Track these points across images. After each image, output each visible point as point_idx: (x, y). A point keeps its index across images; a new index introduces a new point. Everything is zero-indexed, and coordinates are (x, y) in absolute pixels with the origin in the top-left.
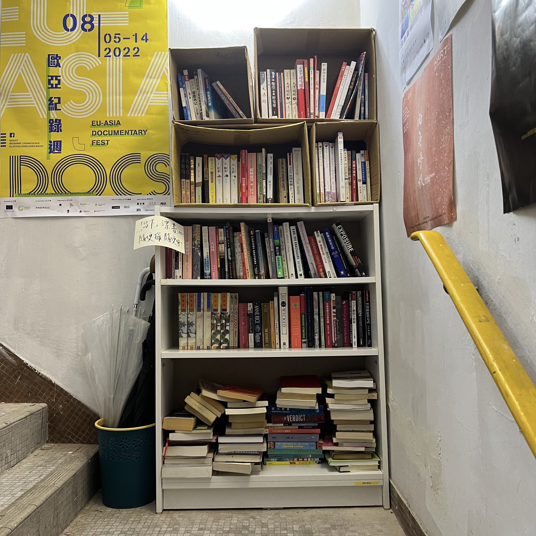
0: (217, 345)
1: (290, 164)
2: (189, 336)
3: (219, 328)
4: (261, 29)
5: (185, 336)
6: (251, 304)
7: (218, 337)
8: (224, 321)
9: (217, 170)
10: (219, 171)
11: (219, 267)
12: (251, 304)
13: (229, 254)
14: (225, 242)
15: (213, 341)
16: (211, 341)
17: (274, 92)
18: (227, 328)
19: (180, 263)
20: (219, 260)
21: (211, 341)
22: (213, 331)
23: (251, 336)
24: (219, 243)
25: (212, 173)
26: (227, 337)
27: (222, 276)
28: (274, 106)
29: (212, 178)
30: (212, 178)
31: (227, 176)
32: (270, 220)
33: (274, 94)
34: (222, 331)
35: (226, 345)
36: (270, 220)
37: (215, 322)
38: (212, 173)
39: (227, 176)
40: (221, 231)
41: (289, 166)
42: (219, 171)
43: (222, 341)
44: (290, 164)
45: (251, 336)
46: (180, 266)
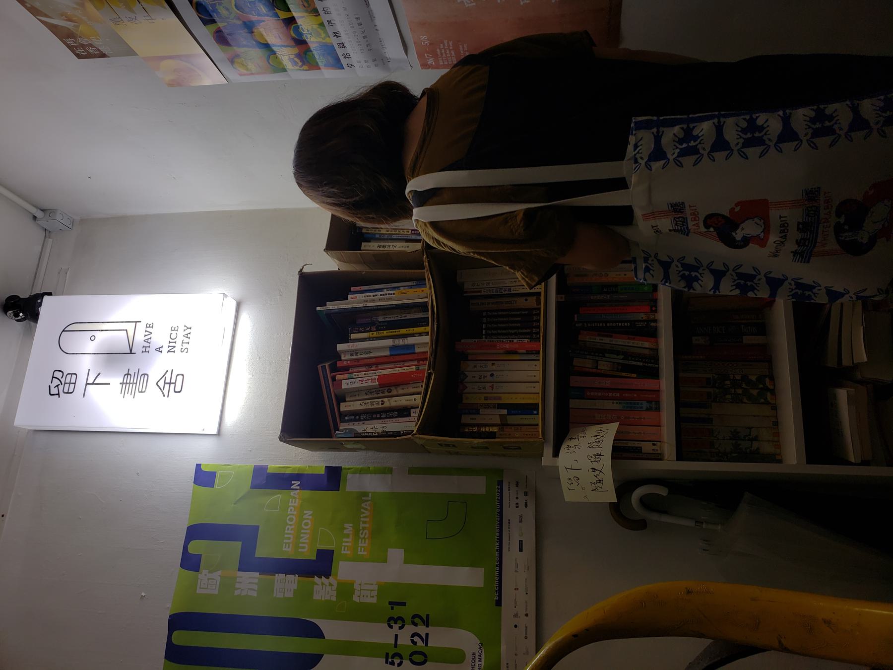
0: (769, 394)
1: (480, 292)
2: (756, 439)
3: (740, 391)
4: (283, 430)
5: (755, 445)
6: (694, 338)
7: (754, 392)
8: (728, 382)
9: (483, 391)
10: (484, 388)
11: (635, 375)
12: (694, 338)
13: (615, 356)
14: (597, 358)
15: (762, 400)
16: (762, 403)
17: (374, 416)
18: (738, 377)
19: (631, 444)
20: (624, 374)
21: (762, 403)
22: (745, 400)
23: (747, 340)
24: (597, 368)
25: (486, 398)
26: (754, 378)
27: (655, 374)
28: (396, 414)
29: (495, 398)
30: (495, 398)
31: (492, 375)
32: (563, 298)
33: (378, 416)
34: (744, 386)
35: (767, 380)
36: (563, 298)
37: (729, 397)
38: (486, 398)
39: (492, 375)
40: (577, 362)
41: (483, 293)
42: (484, 388)
43: (761, 386)
44: (480, 292)
45: (747, 340)
46: (636, 444)
